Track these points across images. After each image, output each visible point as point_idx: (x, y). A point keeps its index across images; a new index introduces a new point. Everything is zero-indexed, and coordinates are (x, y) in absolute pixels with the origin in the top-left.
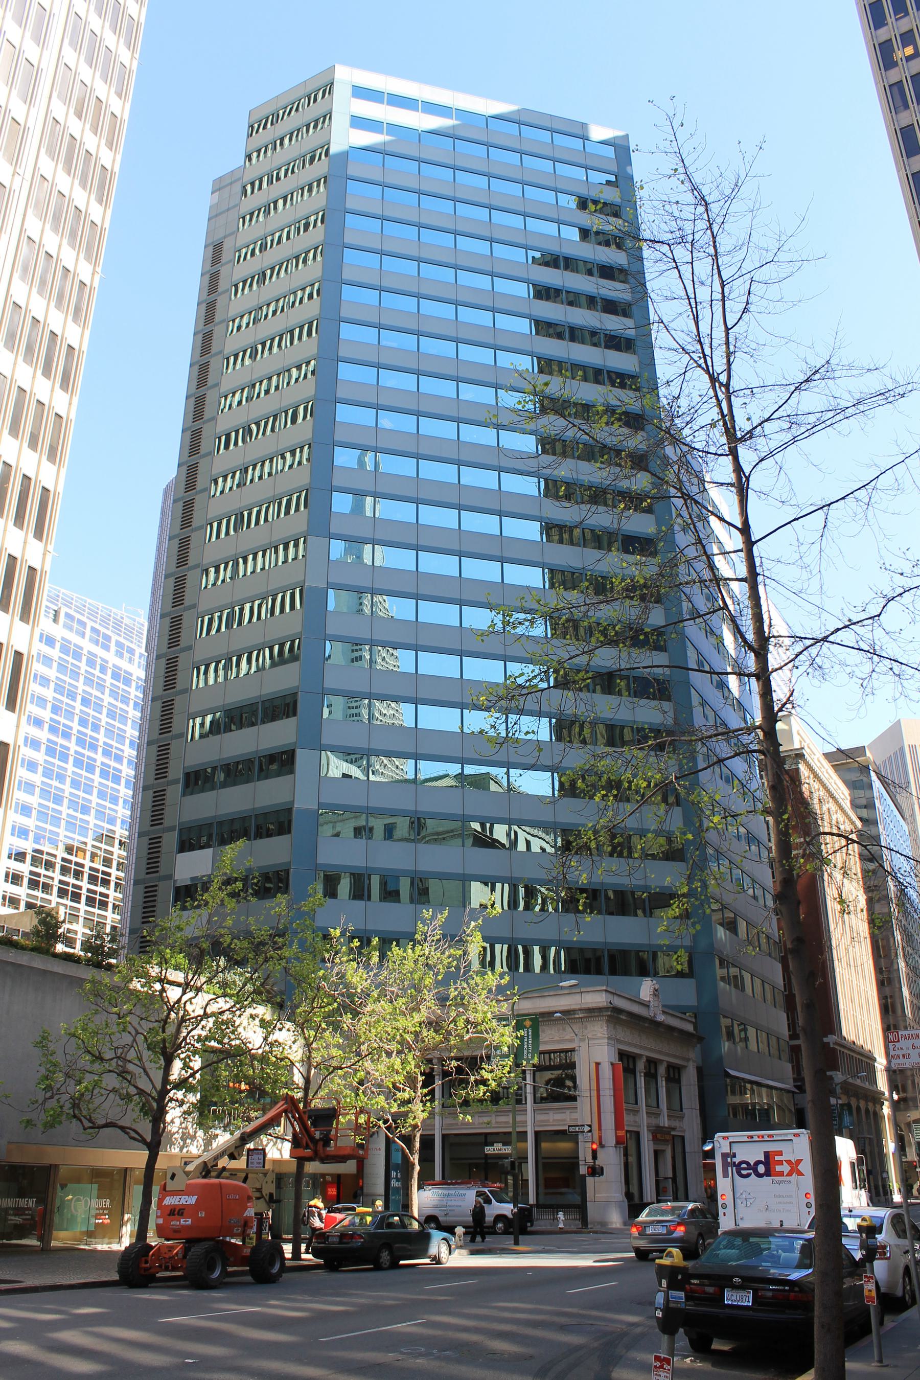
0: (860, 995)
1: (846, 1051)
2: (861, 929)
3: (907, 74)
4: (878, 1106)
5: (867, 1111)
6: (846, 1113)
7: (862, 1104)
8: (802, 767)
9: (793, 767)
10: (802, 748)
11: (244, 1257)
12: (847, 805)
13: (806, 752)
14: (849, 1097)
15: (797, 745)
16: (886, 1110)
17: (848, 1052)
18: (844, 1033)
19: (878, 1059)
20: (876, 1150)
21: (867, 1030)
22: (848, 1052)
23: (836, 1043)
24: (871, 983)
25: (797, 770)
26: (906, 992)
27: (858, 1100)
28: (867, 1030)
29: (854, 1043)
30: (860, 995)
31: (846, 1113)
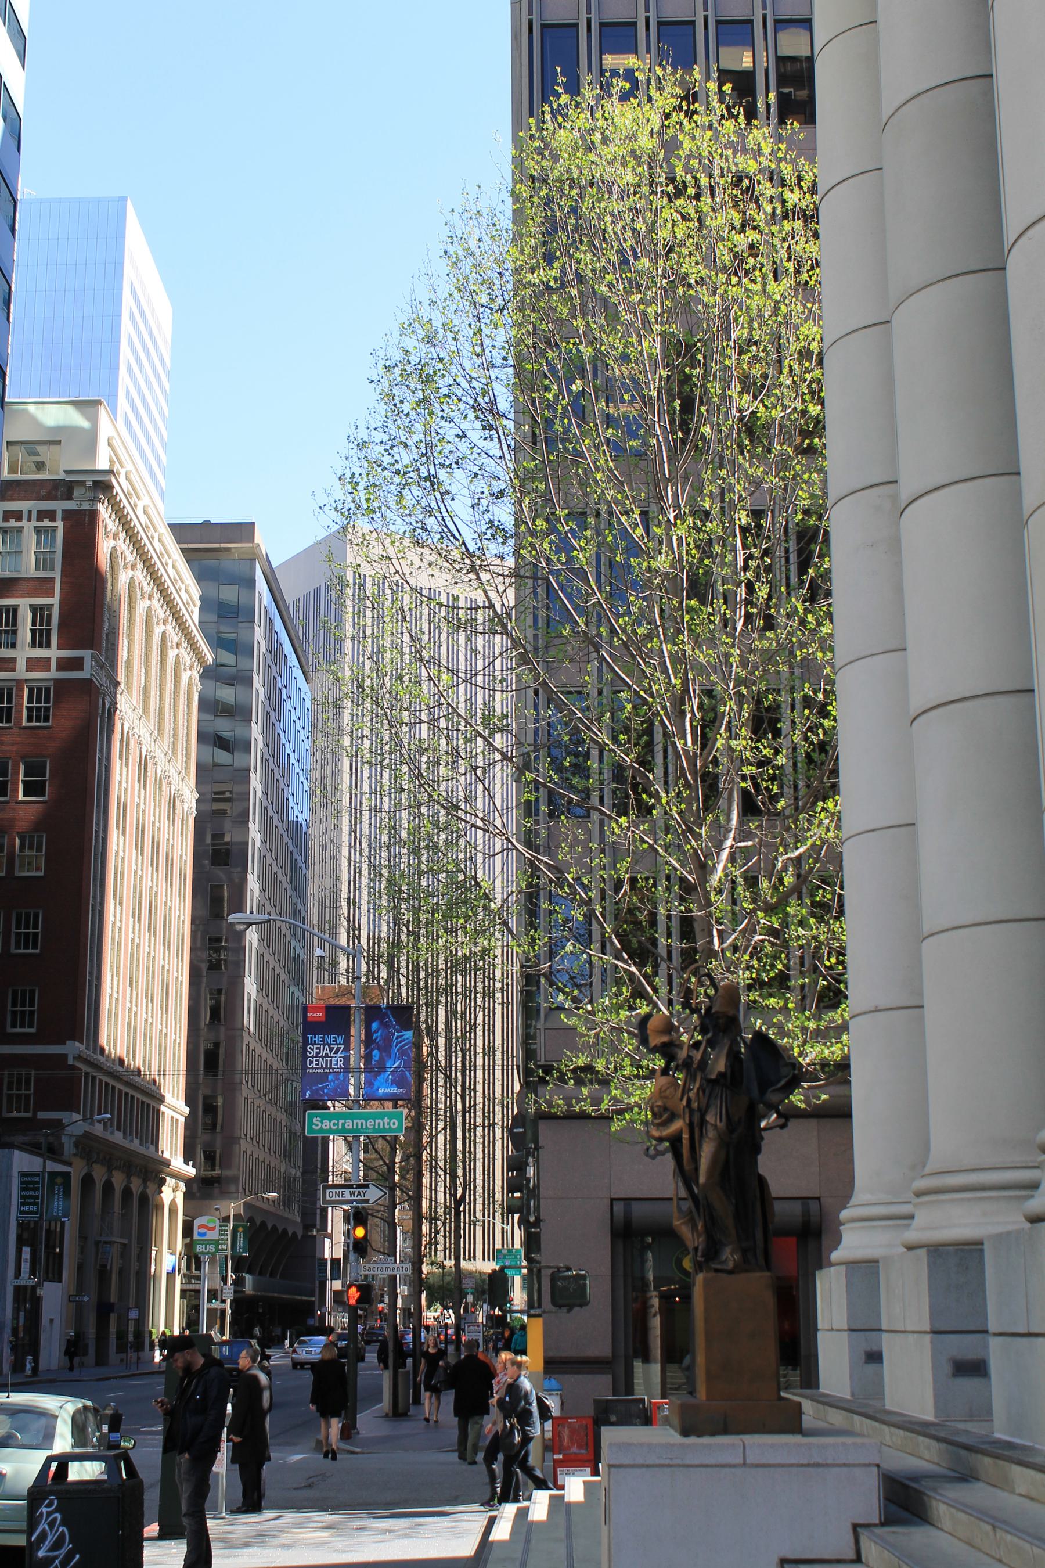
0: (150, 973)
1: (137, 1095)
2: (177, 852)
3: (652, 14)
4: (151, 1187)
5: (127, 1193)
6: (59, 1190)
7: (118, 1180)
8: (104, 511)
9: (86, 506)
10: (111, 472)
11: (338, 1415)
12: (193, 616)
13: (120, 485)
14: (90, 1163)
15: (102, 464)
16: (172, 1194)
17: (125, 1089)
18: (103, 1040)
19: (169, 1098)
20: (134, 1266)
21: (155, 1042)
22: (125, 1089)
23: (79, 1058)
24: (179, 956)
25: (93, 514)
26: (250, 986)
27: (110, 1170)
28: (155, 1042)
29: (121, 1061)
30: (150, 973)
31: (59, 1190)
